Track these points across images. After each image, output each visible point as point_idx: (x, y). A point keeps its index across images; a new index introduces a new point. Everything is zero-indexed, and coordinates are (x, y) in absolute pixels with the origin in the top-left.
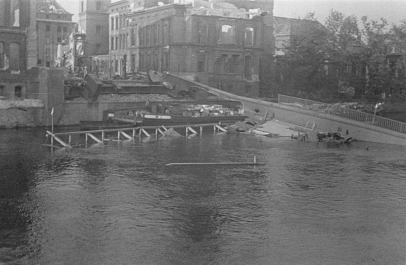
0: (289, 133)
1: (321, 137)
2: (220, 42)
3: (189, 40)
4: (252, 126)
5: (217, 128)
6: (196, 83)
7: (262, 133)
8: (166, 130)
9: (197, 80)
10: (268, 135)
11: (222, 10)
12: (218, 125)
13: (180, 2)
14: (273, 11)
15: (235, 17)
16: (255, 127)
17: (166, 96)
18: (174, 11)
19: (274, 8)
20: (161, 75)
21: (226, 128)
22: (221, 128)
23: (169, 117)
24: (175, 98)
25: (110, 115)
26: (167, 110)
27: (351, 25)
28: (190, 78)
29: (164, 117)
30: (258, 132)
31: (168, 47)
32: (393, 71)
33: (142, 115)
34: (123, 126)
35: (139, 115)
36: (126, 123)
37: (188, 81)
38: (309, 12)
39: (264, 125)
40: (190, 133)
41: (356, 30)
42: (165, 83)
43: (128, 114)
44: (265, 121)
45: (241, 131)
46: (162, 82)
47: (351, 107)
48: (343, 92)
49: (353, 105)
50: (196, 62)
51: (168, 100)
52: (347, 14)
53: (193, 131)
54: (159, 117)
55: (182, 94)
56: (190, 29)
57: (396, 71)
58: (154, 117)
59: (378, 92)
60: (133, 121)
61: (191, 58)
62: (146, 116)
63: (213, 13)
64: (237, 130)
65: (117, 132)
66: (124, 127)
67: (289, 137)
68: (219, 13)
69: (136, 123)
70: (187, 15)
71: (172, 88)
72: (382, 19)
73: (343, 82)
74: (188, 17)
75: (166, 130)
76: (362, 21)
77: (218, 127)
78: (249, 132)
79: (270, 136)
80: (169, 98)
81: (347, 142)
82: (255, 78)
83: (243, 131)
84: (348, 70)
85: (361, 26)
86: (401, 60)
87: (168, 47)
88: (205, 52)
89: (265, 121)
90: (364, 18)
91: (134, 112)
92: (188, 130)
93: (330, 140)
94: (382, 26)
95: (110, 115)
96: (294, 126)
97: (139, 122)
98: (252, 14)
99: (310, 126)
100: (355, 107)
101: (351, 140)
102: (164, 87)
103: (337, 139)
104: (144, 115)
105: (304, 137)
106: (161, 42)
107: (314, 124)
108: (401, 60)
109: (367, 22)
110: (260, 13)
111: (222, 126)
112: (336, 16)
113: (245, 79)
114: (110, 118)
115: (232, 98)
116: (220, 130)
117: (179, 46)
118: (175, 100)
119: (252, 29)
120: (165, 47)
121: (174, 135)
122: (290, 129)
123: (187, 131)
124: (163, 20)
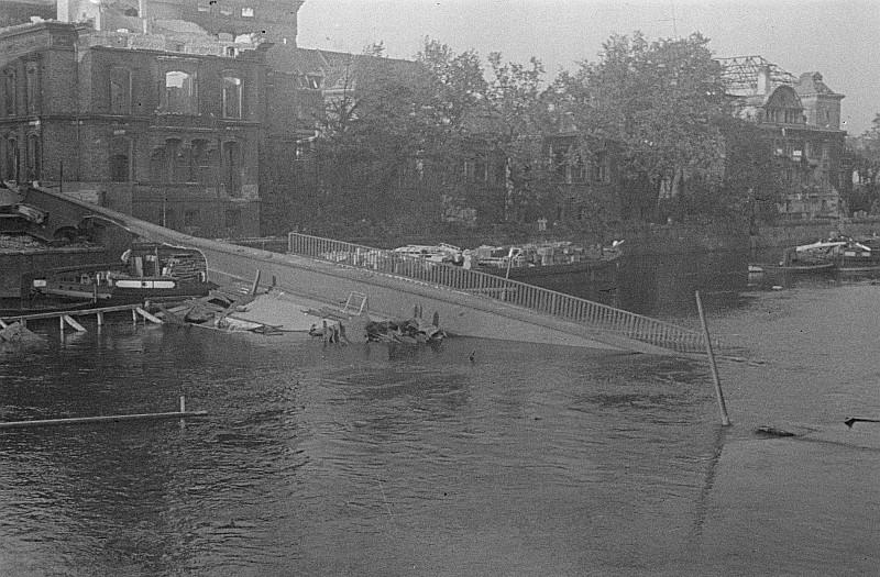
0: (307, 323)
1: (373, 331)
2: (161, 111)
3: (86, 105)
4: (222, 309)
5: (139, 315)
6: (102, 209)
7: (244, 325)
8: (4, 326)
9: (105, 200)
10: (258, 328)
11: (163, 38)
12: (143, 308)
13: (70, 17)
14: (297, 39)
15: (197, 52)
16: (230, 310)
17: (27, 239)
18: (49, 40)
19: (299, 32)
20: (17, 190)
21: (161, 314)
22: (150, 317)
23: (171, 285)
24: (51, 244)
25: (37, 283)
26: (165, 269)
27: (468, 72)
28: (88, 195)
29: (158, 285)
30: (237, 323)
31: (38, 123)
32: (561, 170)
33: (110, 281)
34: (72, 305)
35: (104, 281)
36: (77, 300)
37: (73, 204)
38: (371, 43)
39: (248, 306)
40: (69, 329)
41: (481, 85)
42: (24, 210)
43: (79, 279)
44: (255, 294)
45: (194, 321)
46: (17, 207)
47: (559, 251)
48: (452, 219)
49: (561, 247)
50: (105, 156)
51: (32, 251)
52: (792, 65)
53: (75, 325)
54: (149, 285)
55: (68, 234)
56: (87, 81)
57: (568, 170)
58: (137, 284)
59: (531, 216)
60: (90, 295)
61: (95, 149)
62: (120, 284)
63: (142, 44)
64: (187, 319)
65: (96, 315)
66: (72, 309)
67: (304, 331)
68: (158, 43)
69: (98, 299)
70: (80, 47)
71: (40, 220)
72: (533, 60)
73: (451, 198)
74: (84, 52)
75: (4, 326)
76: (490, 64)
77: (142, 312)
78: (216, 322)
79: (263, 330)
80: (36, 244)
81: (433, 342)
82: (249, 192)
83: (199, 322)
84: (468, 169)
85: (489, 75)
86: (575, 147)
87: (38, 123)
88: (126, 134)
89: (255, 294)
90: (495, 58)
91: (93, 274)
92: (65, 322)
93: (395, 337)
94: (533, 75)
95: (37, 283)
96: (316, 306)
97: (104, 296)
98: (239, 46)
99: (354, 305)
100: (566, 252)
101: (440, 337)
102: (22, 218)
103: (410, 335)
104: (115, 280)
105: (336, 332)
106: (22, 111)
107: (364, 301)
108: (575, 147)
109: (501, 66)
110: (256, 44)
111: (152, 312)
112: (435, 52)
113: (224, 194)
114: (39, 289)
115: (181, 243)
116: (147, 320)
117: (59, 119)
118: (51, 249)
119: (238, 82)
120: (31, 123)
121: (26, 338)
122: (309, 312)
123: (62, 327)
124: (24, 59)
